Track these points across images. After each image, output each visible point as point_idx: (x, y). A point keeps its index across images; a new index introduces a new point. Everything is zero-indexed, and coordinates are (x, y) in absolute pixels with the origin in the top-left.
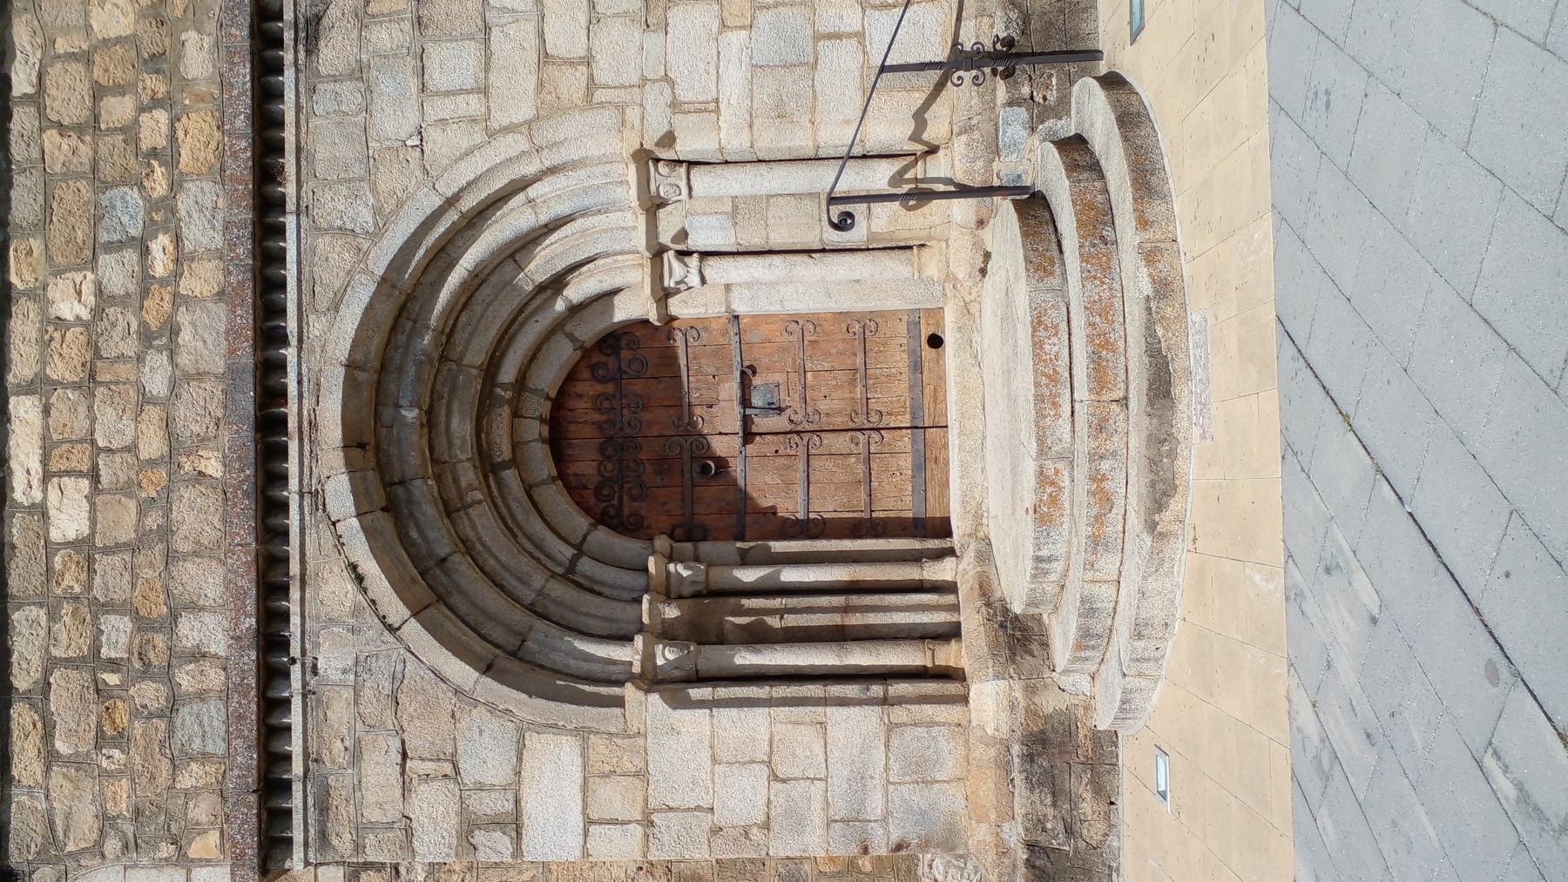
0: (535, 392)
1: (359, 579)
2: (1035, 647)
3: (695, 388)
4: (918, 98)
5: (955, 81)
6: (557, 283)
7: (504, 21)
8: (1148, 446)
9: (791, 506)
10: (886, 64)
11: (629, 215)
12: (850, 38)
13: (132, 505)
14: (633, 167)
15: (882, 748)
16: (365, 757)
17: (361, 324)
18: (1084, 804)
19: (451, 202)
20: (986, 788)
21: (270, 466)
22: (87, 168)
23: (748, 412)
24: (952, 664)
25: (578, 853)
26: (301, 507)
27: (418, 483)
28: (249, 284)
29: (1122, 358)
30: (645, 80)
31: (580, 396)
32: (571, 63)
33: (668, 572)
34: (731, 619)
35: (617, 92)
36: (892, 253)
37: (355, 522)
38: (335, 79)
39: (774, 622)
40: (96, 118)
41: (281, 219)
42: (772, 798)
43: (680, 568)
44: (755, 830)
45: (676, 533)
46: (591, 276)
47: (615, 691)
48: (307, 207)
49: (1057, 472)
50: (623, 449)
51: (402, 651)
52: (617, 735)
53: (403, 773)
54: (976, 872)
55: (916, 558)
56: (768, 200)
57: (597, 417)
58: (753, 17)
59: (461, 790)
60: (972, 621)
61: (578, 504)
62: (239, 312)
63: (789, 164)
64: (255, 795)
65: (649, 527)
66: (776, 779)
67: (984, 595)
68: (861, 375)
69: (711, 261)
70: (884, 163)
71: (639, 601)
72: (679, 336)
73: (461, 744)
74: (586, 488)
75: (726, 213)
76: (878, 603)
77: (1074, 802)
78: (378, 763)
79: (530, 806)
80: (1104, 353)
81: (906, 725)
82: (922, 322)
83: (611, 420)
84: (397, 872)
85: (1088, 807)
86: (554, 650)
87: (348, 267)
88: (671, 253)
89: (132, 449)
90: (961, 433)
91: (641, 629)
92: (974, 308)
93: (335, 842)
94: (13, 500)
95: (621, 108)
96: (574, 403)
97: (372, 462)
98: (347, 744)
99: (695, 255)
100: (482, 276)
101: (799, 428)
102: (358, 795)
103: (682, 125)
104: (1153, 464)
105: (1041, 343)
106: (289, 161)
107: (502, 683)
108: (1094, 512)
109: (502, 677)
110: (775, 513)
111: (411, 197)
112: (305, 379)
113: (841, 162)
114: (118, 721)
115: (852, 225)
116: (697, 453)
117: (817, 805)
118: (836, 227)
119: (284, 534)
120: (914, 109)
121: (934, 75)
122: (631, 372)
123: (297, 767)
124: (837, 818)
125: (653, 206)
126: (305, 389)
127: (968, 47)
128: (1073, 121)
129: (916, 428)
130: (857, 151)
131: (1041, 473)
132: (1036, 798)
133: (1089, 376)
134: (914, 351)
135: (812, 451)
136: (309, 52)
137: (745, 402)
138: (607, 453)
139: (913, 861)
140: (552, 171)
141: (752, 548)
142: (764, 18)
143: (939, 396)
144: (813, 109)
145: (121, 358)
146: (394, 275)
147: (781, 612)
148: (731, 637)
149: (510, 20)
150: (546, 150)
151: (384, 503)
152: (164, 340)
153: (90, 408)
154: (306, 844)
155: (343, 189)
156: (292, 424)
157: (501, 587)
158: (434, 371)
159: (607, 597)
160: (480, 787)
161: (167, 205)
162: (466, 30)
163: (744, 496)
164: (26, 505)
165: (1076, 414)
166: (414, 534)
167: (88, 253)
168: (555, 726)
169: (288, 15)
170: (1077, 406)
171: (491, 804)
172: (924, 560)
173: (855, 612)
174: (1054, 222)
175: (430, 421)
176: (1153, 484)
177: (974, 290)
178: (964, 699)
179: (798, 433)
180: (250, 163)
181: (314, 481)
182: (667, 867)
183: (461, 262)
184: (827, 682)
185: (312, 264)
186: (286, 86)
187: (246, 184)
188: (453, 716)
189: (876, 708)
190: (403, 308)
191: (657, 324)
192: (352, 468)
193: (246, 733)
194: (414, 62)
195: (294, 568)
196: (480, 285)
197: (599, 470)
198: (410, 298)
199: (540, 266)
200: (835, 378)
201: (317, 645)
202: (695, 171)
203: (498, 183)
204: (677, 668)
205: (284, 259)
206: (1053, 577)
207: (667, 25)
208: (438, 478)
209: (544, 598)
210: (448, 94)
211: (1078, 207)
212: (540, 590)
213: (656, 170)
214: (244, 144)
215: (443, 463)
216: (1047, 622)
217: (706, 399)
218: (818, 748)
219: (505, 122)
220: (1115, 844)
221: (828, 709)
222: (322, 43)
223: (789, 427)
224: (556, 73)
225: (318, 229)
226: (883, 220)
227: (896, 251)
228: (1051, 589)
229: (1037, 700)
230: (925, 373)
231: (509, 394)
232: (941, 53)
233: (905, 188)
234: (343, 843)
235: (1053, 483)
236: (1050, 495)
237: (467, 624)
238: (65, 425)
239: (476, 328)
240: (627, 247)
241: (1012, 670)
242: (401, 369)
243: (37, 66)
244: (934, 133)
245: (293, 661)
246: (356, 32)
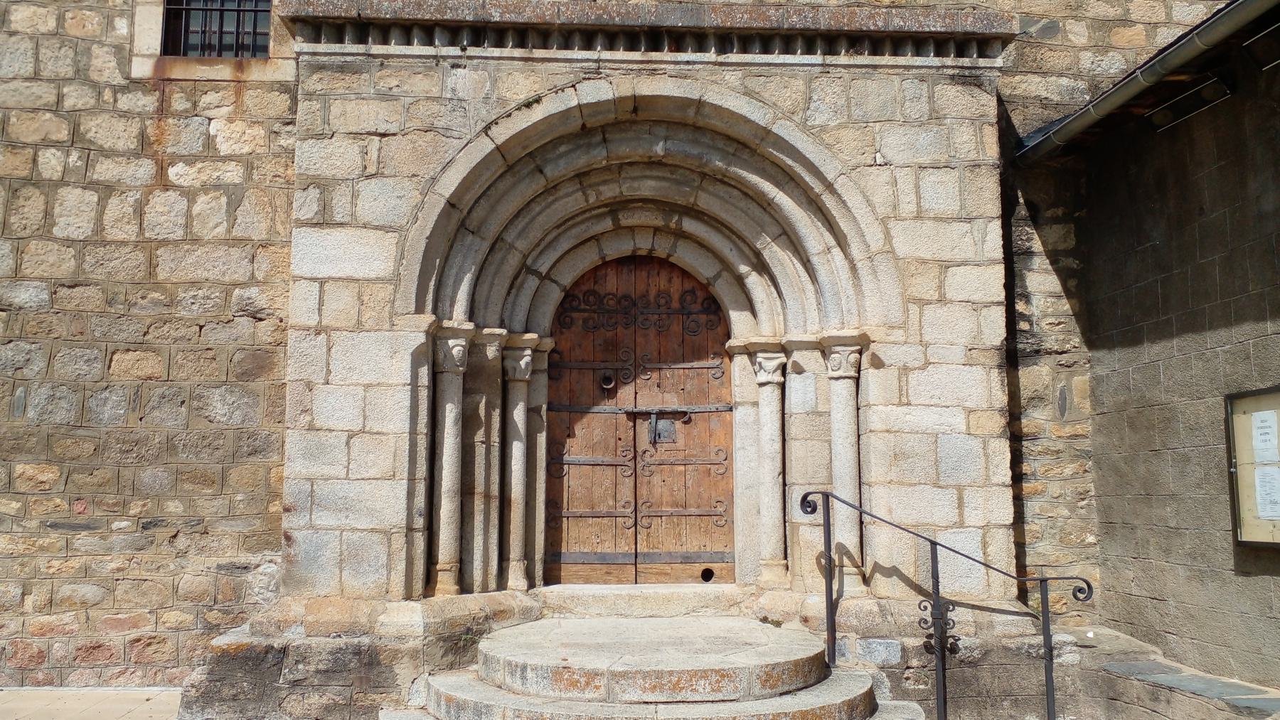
0: (674, 246)
1: (528, 105)
2: (450, 658)
3: (674, 373)
4: (909, 571)
5: (924, 604)
6: (762, 267)
7: (976, 234)
9: (575, 450)
10: (938, 547)
11: (816, 327)
12: (959, 515)
14: (855, 333)
15: (371, 527)
16: (383, 104)
17: (733, 113)
18: (317, 697)
19: (830, 187)
20: (333, 614)
21: (621, 36)
23: (654, 417)
24: (438, 586)
25: (297, 272)
26: (588, 60)
27: (604, 153)
28: (768, 25)
30: (926, 346)
31: (670, 281)
32: (941, 286)
33: (524, 349)
34: (484, 401)
35: (917, 323)
36: (782, 542)
37: (574, 103)
38: (931, 98)
39: (480, 436)
41: (819, 52)
42: (334, 433)
43: (527, 359)
44: (308, 418)
45: (556, 355)
46: (767, 295)
47: (429, 306)
48: (828, 72)
49: (597, 687)
50: (626, 314)
51: (469, 137)
52: (392, 307)
53: (369, 133)
54: (264, 600)
55: (528, 555)
56: (827, 441)
57: (653, 293)
58: (976, 436)
59: (353, 179)
60: (474, 603)
61: (583, 276)
62: (746, 16)
63: (856, 460)
64: (356, 15)
65: (562, 333)
66: (350, 437)
67: (495, 614)
68: (681, 511)
69: (777, 392)
70: (856, 540)
71: (501, 326)
72: (717, 362)
73: (390, 181)
74: (596, 283)
75: (816, 406)
76: (491, 523)
78: (378, 113)
81: (389, 547)
82: (724, 565)
83: (649, 304)
84: (288, 124)
86: (465, 257)
87: (779, 104)
88: (784, 360)
90: (631, 597)
91: (479, 327)
92: (734, 610)
93: (315, 77)
95: (904, 326)
96: (664, 275)
97: (621, 117)
98: (395, 90)
99: (783, 379)
100: (768, 209)
101: (639, 459)
102: (353, 97)
103: (889, 375)
106: (865, 59)
107: (440, 216)
109: (444, 216)
110: (569, 436)
111: (835, 156)
112: (690, 67)
113: (857, 504)
115: (806, 512)
116: (621, 374)
117: (327, 470)
118: (805, 498)
119: (567, 46)
120: (900, 567)
121: (928, 585)
122: (688, 323)
123: (377, 49)
124: (315, 487)
125: (824, 348)
126: (682, 66)
127: (950, 615)
128: (888, 702)
129: (636, 557)
130: (866, 518)
131: (597, 674)
132: (324, 656)
134: (700, 557)
135: (619, 469)
136: (952, 77)
137: (661, 415)
138: (623, 300)
139: (275, 547)
140: (853, 268)
141: (541, 417)
142: (976, 444)
143: (662, 577)
144: (901, 483)
146: (772, 140)
147: (487, 442)
148: (469, 400)
149: (976, 239)
150: (870, 265)
151: (588, 126)
154: (315, 54)
155: (842, 101)
156: (654, 55)
157: (517, 215)
158: (693, 168)
159: (506, 299)
160: (355, 196)
162: (969, 203)
163: (585, 412)
165: (645, 706)
166: (562, 149)
168: (402, 257)
169: (982, 62)
170: (652, 707)
171: (340, 204)
172: (526, 562)
173: (485, 504)
174: (806, 688)
175: (654, 163)
177: (750, 612)
178: (408, 597)
179: (635, 458)
180: (865, 29)
181: (608, 71)
183: (781, 193)
184: (428, 480)
185: (782, 75)
186: (925, 58)
187: (848, 25)
188: (414, 175)
189: (404, 522)
190: (744, 145)
191: (727, 345)
192: (618, 102)
193: (407, 10)
194: (943, 161)
195: (539, 53)
196: (762, 207)
197: (609, 294)
198: (753, 152)
199: (776, 254)
200: (679, 490)
201: (476, 69)
202: (851, 383)
203: (844, 225)
204: (445, 356)
205: (787, 53)
206: (508, 680)
207: (971, 365)
208: (607, 168)
209: (507, 250)
210: (917, 187)
211: (818, 711)
212: (514, 246)
213: (853, 352)
214: (880, 24)
216: (470, 668)
217: (665, 383)
218: (373, 473)
219: (893, 233)
221: (405, 482)
222: (960, 88)
223: (640, 450)
224: (933, 274)
225: (811, 81)
226: (809, 536)
227: (783, 546)
228: (498, 677)
229: (406, 659)
230: (682, 566)
231: (673, 225)
232: (946, 591)
233: (835, 557)
234: (313, 83)
235: (588, 684)
236: (578, 681)
237: (488, 188)
239: (727, 202)
240: (790, 324)
241: (431, 638)
242: (696, 142)
244: (879, 581)
245: (464, 49)
246: (969, 115)
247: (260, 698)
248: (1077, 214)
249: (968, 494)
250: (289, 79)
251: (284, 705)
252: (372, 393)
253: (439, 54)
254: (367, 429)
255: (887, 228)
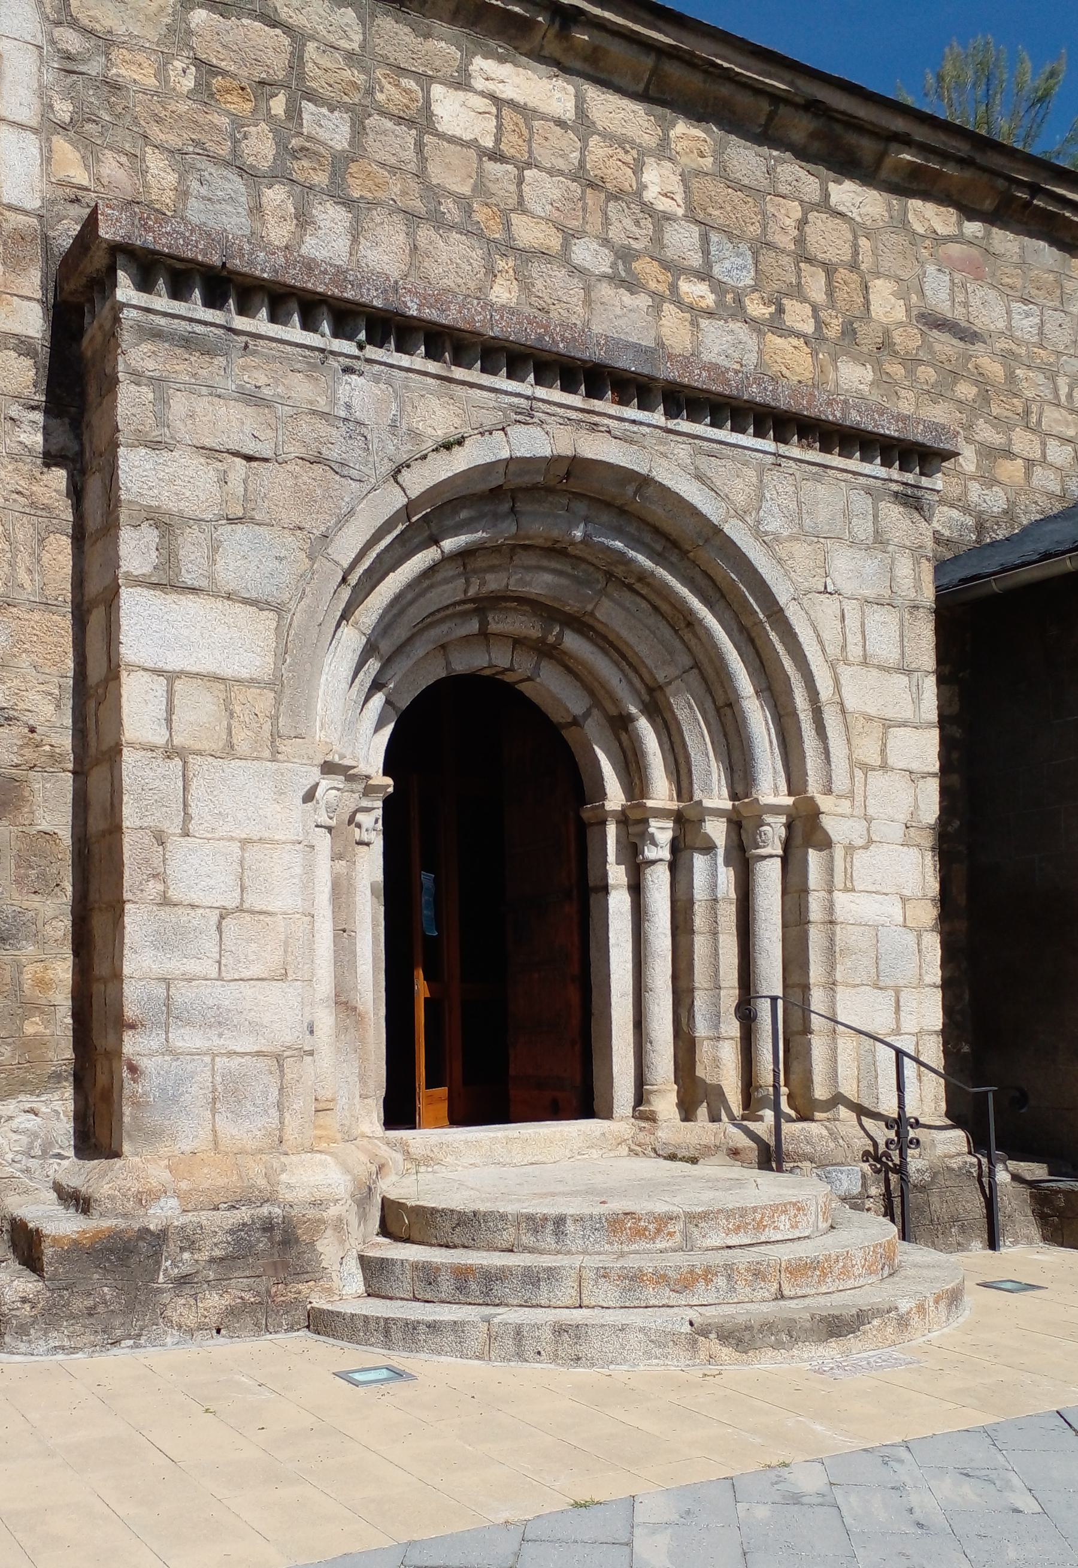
1: (448, 446)
8: (784, 1320)
13: (466, 189)
15: (256, 1048)
16: (249, 410)
18: (217, 1298)
19: (777, 614)
22: (770, 238)
29: (813, 1291)
37: (505, 454)
40: (809, 260)
44: (161, 887)
49: (671, 1234)
64: (219, 264)
66: (222, 917)
77: (220, 1284)
79: (190, 604)
80: (818, 1273)
81: (282, 1077)
85: (214, 1301)
89: (521, 206)
94: (474, 54)
100: (688, 636)
102: (204, 391)
104: (768, 1327)
105: (785, 1212)
108: (670, 1273)
112: (635, 428)
114: (229, 97)
117: (193, 967)
124: (172, 991)
132: (220, 1237)
133: (800, 1259)
136: (896, 494)
142: (910, 938)
145: (607, 222)
152: (623, 274)
153: (561, 173)
154: (148, 310)
160: (215, 547)
161: (738, 312)
164: (471, 68)
166: (464, 514)
167: (701, 216)
169: (925, 482)
175: (556, 551)
176: (748, 1328)
180: (823, 417)
182: (35, 766)
192: (554, 460)
198: (684, 553)
201: (377, 379)
215: (511, 558)
218: (256, 970)
220: (169, 1340)
222: (902, 509)
235: (659, 1231)
236: (646, 1229)
238: (546, 139)
243: (850, 214)
247: (130, 1309)
248: (961, 675)
249: (903, 996)
250: (32, 333)
251: (168, 1313)
252: (253, 854)
253: (328, 348)
254: (246, 906)
255: (835, 673)
